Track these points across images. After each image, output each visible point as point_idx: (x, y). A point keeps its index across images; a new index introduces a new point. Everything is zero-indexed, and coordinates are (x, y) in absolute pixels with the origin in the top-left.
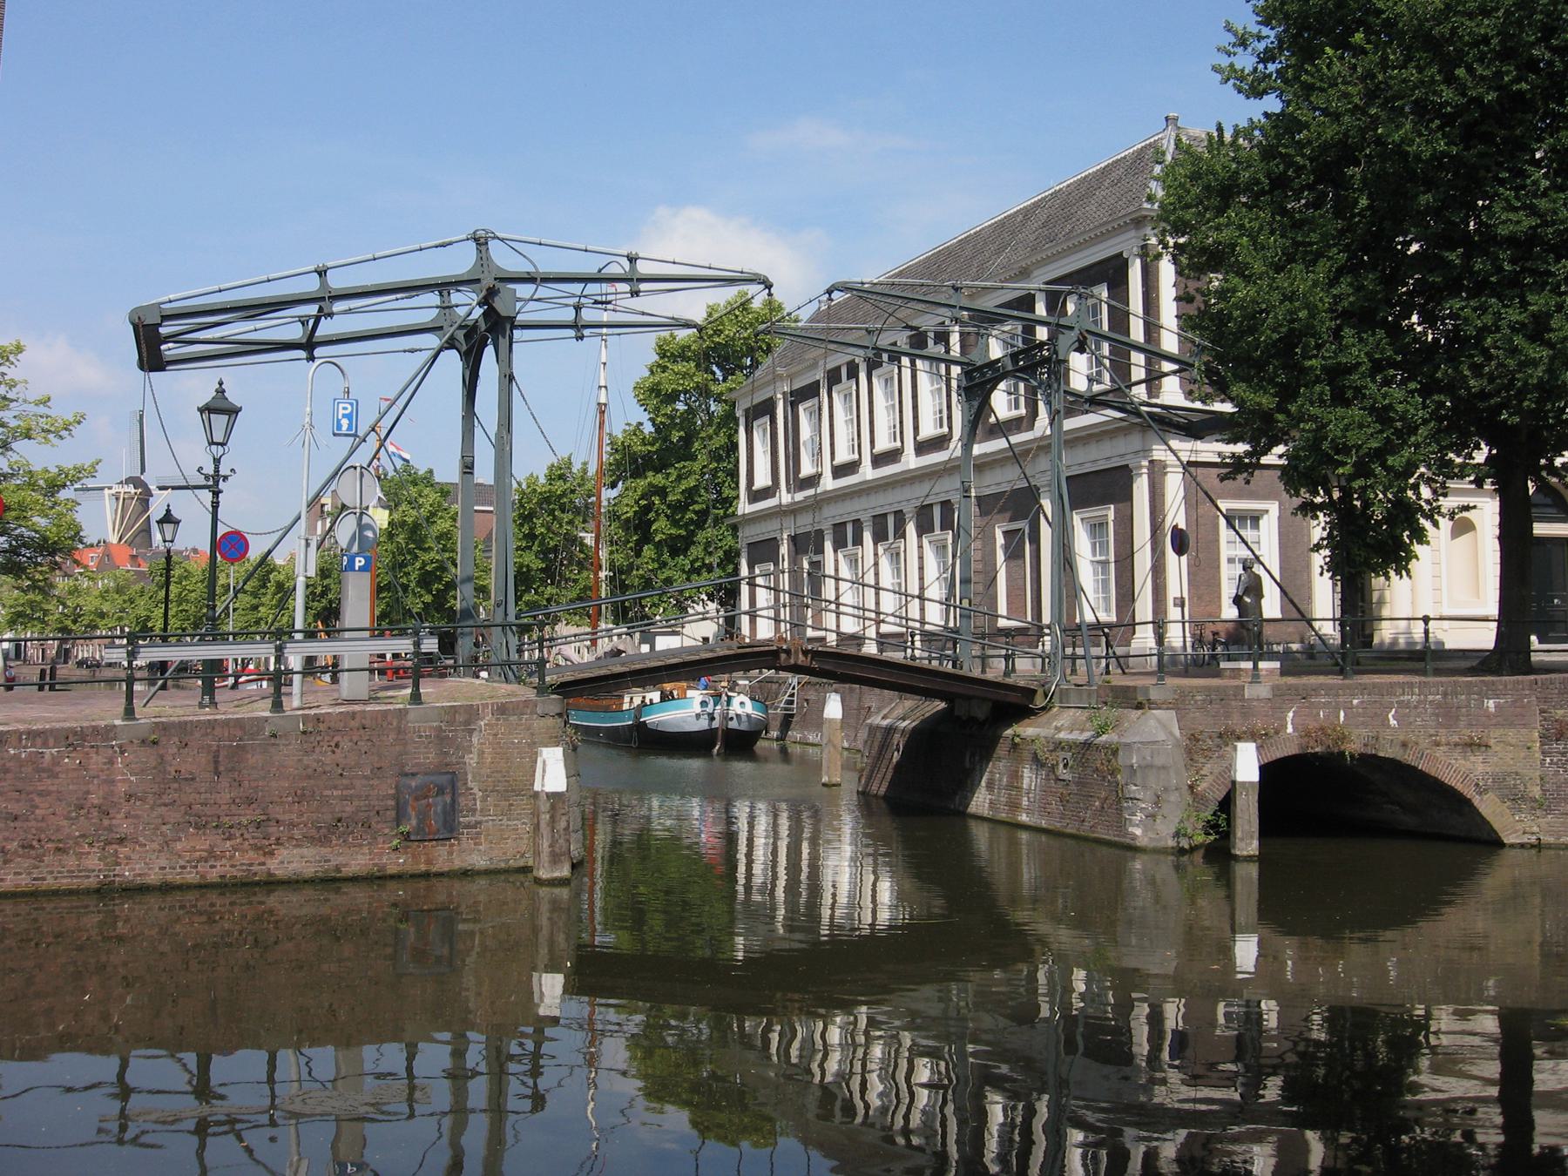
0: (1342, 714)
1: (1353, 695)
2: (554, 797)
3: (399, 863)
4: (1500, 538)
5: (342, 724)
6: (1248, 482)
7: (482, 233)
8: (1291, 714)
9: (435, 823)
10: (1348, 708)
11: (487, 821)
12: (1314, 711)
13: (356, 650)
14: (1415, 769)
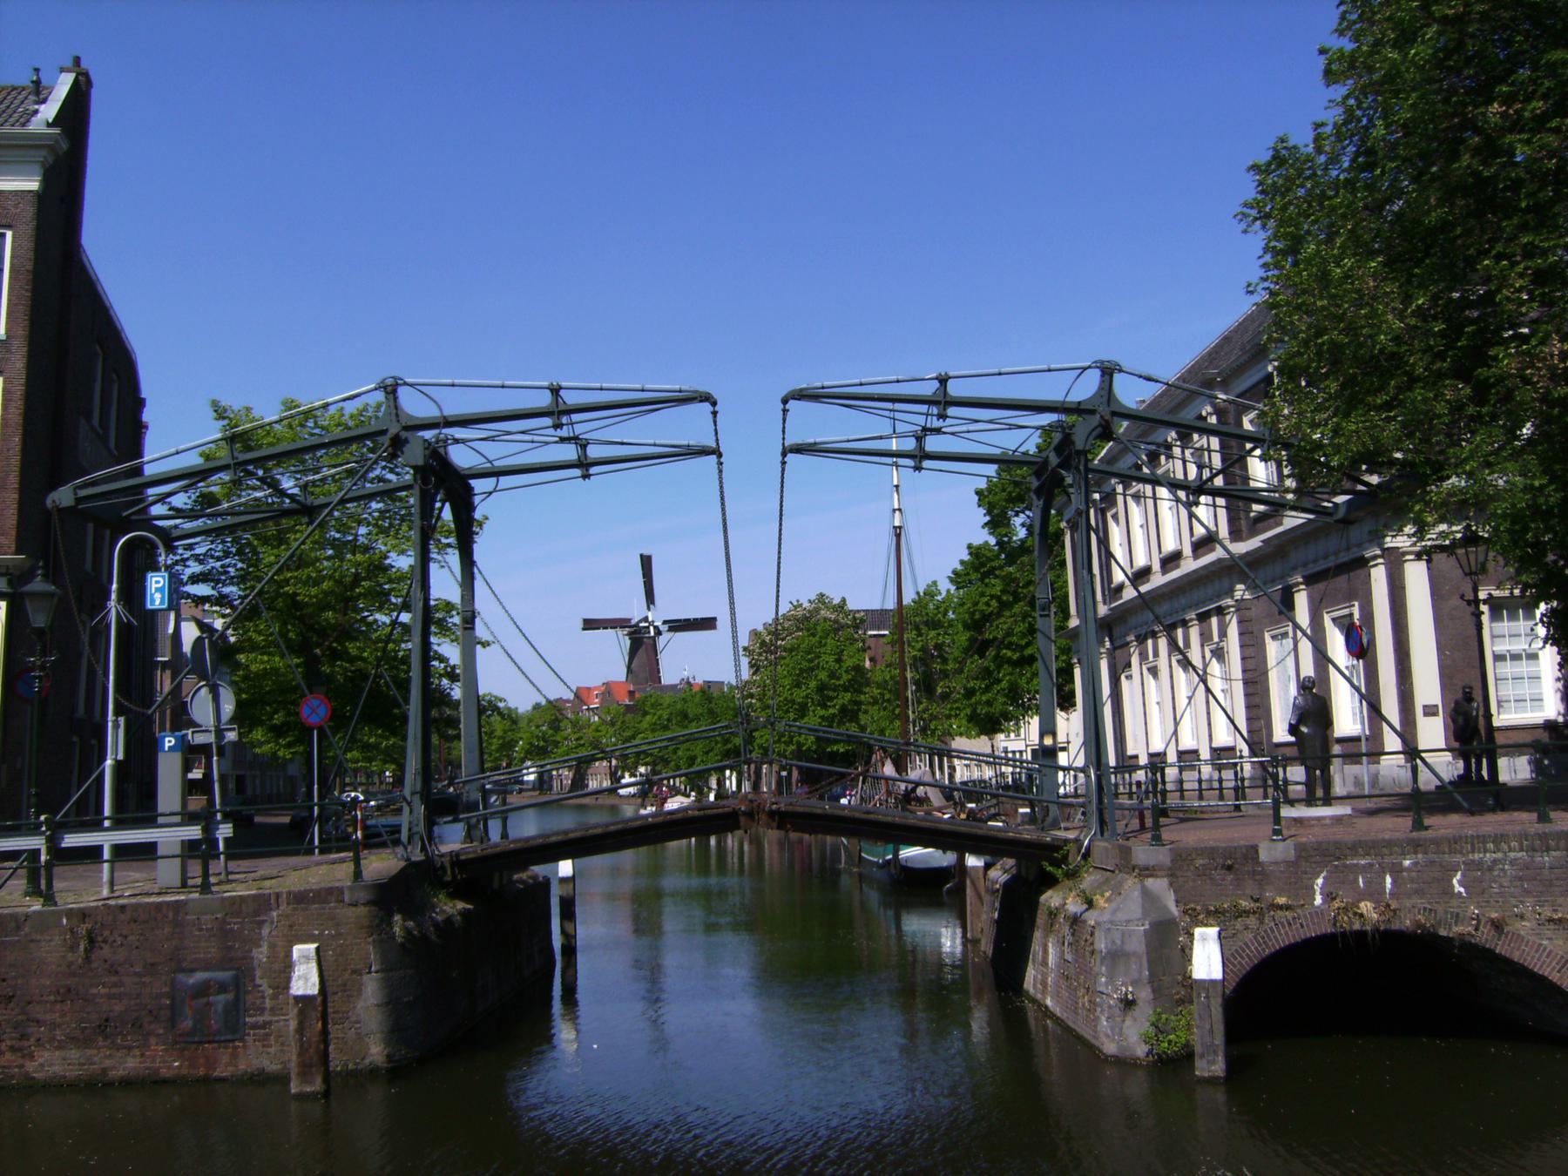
0: (1388, 880)
1: (1404, 855)
2: (304, 1000)
3: (175, 1066)
4: (141, 403)
5: (111, 918)
6: (1462, 597)
7: (389, 382)
8: (1320, 881)
9: (215, 1023)
10: (1396, 871)
11: (277, 1021)
12: (1351, 877)
13: (170, 836)
14: (1491, 952)
